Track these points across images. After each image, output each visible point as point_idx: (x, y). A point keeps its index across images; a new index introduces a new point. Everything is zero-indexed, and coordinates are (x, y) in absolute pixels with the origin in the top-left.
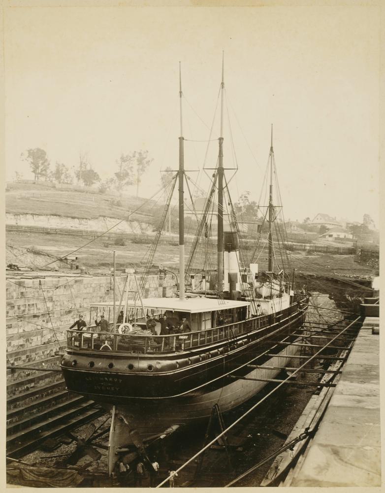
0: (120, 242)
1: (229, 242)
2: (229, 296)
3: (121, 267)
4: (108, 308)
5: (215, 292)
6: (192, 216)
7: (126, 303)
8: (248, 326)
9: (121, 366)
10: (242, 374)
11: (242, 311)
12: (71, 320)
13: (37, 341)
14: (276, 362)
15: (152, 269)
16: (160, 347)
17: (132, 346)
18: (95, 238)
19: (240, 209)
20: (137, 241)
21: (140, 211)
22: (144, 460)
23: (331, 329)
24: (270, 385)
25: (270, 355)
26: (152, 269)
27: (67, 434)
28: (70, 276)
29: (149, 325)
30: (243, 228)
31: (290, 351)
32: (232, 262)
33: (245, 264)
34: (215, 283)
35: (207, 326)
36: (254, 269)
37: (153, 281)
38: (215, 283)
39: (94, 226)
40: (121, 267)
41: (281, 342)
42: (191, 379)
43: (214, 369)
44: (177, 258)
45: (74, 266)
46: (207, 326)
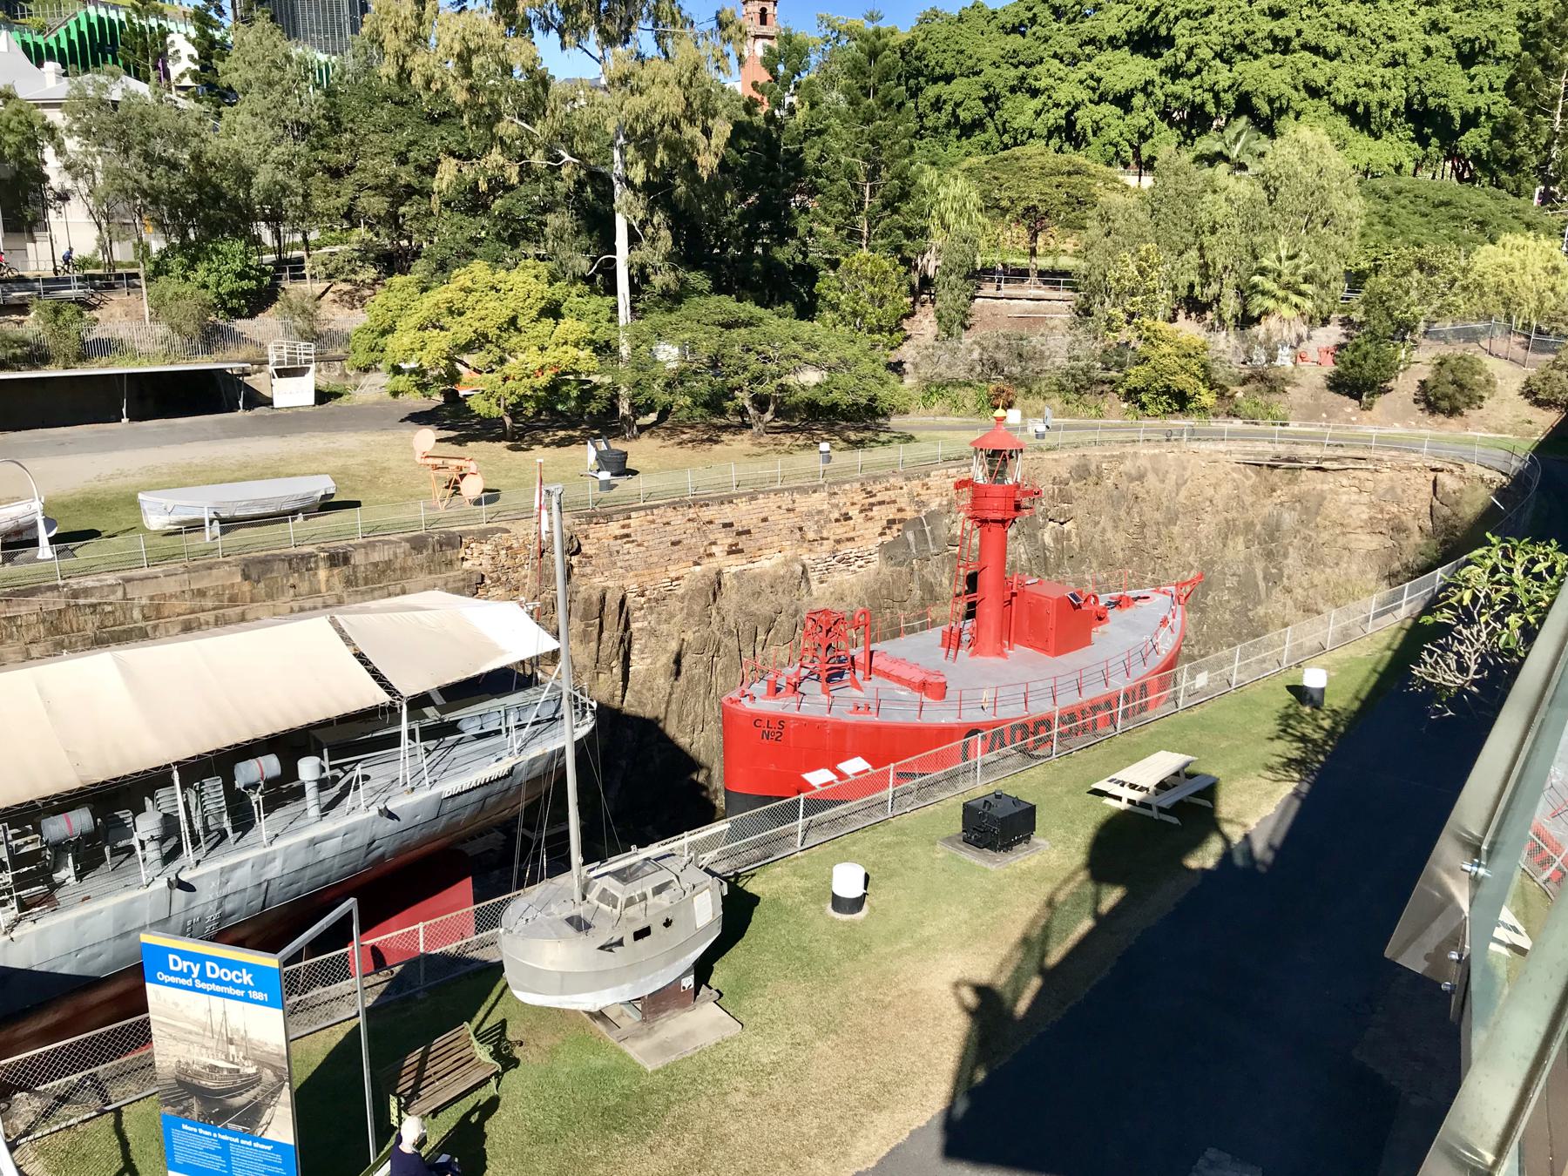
0: (190, 1033)
1: (231, 1042)
2: (233, 1063)
3: (192, 1043)
4: (189, 1058)
5: (227, 1060)
6: (217, 1028)
7: (195, 1057)
8: (241, 1076)
9: (195, 1081)
10: (241, 1094)
11: (238, 1071)
12: (176, 1059)
13: (164, 1065)
14: (253, 1093)
15: (203, 1046)
16: (210, 1078)
17: (198, 1074)
18: (181, 1029)
19: (1029, 228)
20: (197, 1034)
21: (196, 1022)
22: (473, 1119)
23: (273, 1085)
24: (251, 1102)
25: (1175, 820)
26: (203, 1046)
27: (180, 1103)
28: (174, 1042)
29: (204, 1068)
30: (236, 1037)
31: (257, 1089)
32: (232, 1049)
33: (238, 1051)
34: (227, 1056)
35: (225, 1073)
36: (241, 1054)
37: (204, 1050)
38: (227, 1056)
39: (179, 1024)
40: (192, 1043)
41: (1450, 713)
42: (221, 1092)
43: (229, 1091)
44: (212, 1044)
45: (175, 1039)
46: (225, 1073)
